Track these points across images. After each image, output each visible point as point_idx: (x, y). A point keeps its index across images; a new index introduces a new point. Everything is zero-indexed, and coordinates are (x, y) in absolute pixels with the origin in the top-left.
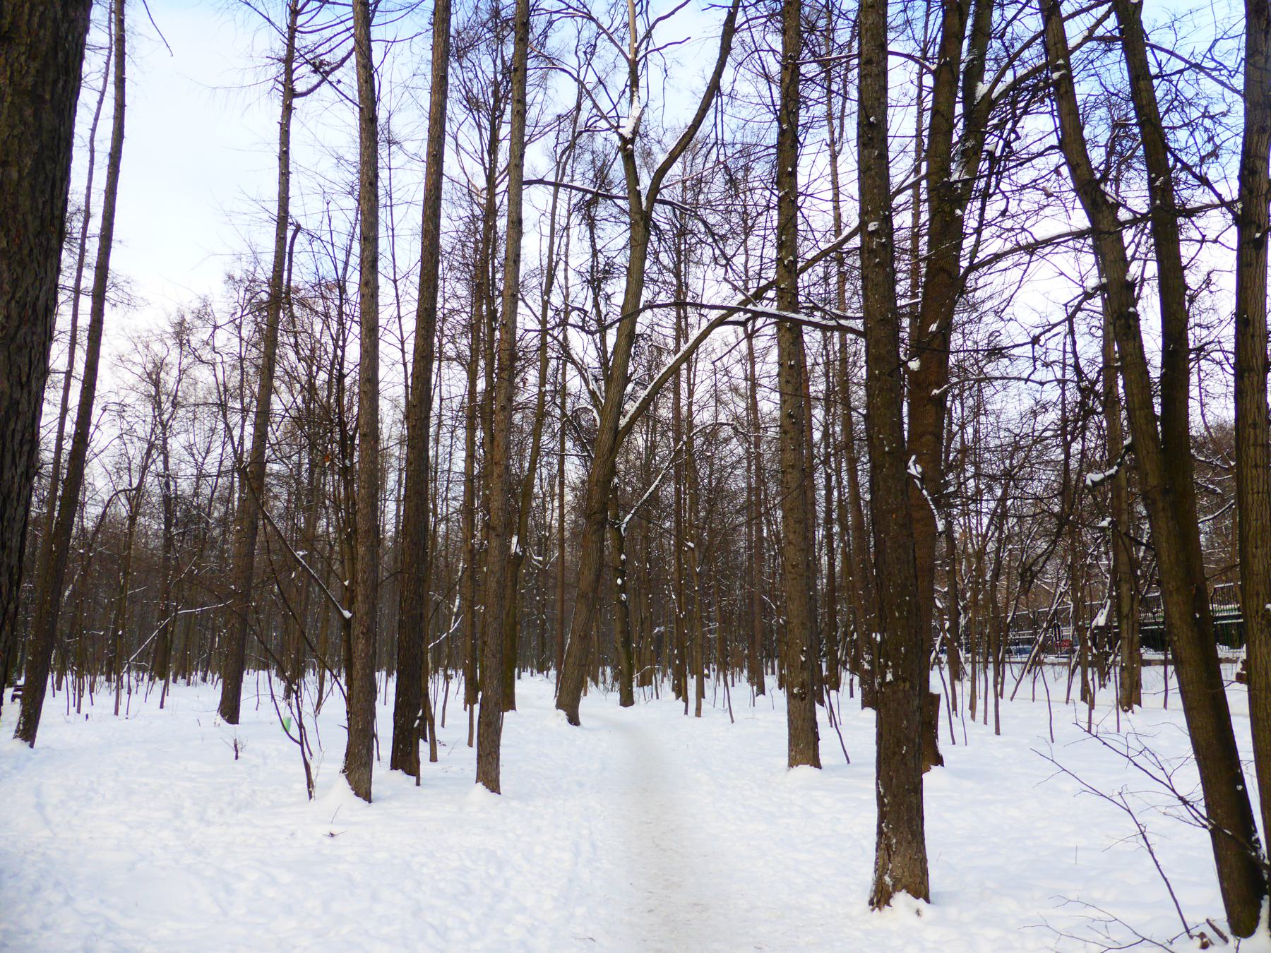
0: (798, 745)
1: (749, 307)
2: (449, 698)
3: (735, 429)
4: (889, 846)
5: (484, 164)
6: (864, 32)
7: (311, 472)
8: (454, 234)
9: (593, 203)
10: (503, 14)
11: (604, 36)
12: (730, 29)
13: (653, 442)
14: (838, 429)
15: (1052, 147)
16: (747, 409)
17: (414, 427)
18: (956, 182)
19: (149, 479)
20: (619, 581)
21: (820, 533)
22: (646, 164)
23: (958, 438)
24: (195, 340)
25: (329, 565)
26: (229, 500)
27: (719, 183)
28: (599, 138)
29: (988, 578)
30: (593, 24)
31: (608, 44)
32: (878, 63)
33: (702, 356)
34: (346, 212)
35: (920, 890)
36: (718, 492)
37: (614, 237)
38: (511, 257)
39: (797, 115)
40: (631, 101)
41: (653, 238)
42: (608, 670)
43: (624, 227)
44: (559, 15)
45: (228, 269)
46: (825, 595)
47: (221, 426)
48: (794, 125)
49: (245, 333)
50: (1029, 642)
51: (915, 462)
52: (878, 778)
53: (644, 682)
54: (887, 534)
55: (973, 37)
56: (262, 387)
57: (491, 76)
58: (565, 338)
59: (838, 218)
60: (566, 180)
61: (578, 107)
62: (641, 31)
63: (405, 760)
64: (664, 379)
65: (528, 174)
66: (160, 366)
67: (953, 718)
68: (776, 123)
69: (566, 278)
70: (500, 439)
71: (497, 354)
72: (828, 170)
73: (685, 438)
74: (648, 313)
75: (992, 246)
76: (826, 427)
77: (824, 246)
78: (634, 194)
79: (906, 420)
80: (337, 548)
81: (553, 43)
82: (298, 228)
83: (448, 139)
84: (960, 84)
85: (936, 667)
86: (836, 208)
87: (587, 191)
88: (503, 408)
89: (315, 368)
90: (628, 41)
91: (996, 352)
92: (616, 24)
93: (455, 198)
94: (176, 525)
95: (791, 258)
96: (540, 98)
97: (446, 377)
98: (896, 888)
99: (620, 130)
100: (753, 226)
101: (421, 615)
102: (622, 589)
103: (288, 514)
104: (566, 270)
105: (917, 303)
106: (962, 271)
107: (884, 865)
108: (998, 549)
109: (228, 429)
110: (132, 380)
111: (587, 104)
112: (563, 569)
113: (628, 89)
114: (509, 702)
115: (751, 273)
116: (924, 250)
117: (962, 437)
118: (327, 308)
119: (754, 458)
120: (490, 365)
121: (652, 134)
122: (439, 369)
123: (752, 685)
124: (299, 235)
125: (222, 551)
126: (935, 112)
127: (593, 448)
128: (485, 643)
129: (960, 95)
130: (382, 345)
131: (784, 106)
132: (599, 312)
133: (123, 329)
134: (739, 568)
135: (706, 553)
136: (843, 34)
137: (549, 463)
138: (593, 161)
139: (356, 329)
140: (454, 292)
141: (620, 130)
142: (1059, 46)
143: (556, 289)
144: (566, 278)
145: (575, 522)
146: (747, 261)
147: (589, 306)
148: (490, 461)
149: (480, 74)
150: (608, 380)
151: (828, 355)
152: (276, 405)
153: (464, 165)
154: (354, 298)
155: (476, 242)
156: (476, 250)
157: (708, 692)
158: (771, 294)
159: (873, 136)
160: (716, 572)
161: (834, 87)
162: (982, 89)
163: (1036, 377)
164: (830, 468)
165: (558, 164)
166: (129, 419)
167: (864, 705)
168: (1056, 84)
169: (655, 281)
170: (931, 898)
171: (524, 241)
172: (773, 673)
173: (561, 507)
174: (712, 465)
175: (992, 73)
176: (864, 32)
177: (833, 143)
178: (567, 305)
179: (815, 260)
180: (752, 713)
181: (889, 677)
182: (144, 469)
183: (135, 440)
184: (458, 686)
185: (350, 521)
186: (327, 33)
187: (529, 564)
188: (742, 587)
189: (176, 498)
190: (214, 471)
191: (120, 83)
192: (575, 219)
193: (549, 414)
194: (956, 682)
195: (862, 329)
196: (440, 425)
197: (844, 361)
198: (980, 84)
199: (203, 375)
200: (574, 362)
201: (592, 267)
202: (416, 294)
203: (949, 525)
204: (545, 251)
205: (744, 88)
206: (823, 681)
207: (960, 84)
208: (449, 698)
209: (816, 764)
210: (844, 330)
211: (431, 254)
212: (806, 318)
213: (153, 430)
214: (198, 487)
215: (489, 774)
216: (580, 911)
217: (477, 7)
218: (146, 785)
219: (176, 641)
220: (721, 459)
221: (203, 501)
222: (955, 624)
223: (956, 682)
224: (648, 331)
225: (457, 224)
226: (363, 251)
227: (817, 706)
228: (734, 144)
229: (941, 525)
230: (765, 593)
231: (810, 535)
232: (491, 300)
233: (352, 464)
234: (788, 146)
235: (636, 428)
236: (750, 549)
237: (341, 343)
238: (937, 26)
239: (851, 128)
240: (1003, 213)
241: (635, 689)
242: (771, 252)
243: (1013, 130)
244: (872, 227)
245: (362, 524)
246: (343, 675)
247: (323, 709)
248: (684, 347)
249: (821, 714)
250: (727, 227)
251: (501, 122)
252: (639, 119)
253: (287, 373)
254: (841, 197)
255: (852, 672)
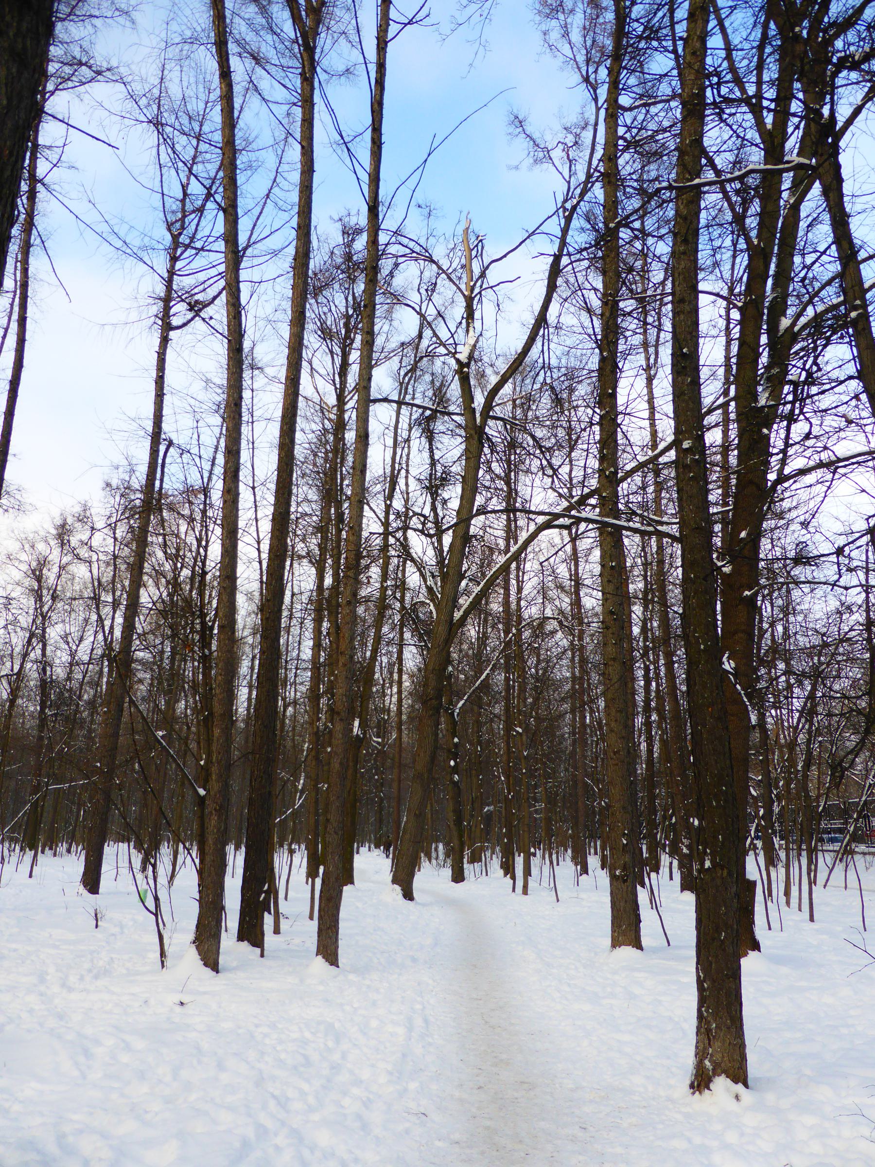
0: (620, 927)
1: (573, 513)
2: (292, 870)
3: (560, 623)
4: (708, 1031)
5: (335, 384)
6: (676, 275)
7: (172, 658)
8: (307, 446)
9: (432, 418)
10: (355, 258)
11: (443, 276)
12: (555, 271)
13: (484, 633)
14: (655, 624)
15: (850, 378)
16: (571, 604)
17: (267, 619)
18: (763, 407)
19: (29, 665)
20: (452, 763)
21: (639, 720)
22: (480, 384)
23: (768, 635)
24: (74, 541)
25: (186, 745)
26: (98, 684)
27: (546, 400)
28: (438, 362)
29: (799, 768)
30: (434, 266)
31: (447, 283)
32: (690, 302)
33: (530, 556)
34: (213, 427)
35: (739, 1076)
36: (544, 681)
37: (451, 448)
38: (359, 467)
39: (616, 344)
40: (467, 331)
41: (486, 450)
42: (441, 846)
43: (460, 440)
44: (404, 259)
45: (106, 478)
46: (644, 779)
47: (94, 617)
48: (613, 354)
49: (119, 534)
50: (840, 831)
51: (729, 658)
52: (697, 963)
53: (475, 859)
54: (704, 726)
55: (776, 277)
56: (132, 582)
57: (343, 310)
58: (406, 539)
59: (654, 434)
60: (408, 398)
61: (420, 336)
62: (477, 271)
63: (251, 933)
64: (495, 577)
65: (374, 394)
66: (43, 563)
67: (769, 903)
68: (597, 351)
69: (407, 485)
70: (345, 632)
71: (342, 549)
72: (645, 391)
73: (514, 631)
74: (482, 518)
75: (796, 464)
76: (644, 622)
77: (641, 459)
78: (469, 410)
79: (719, 617)
80: (193, 729)
81: (398, 282)
82: (170, 444)
83: (305, 364)
84: (765, 317)
85: (751, 853)
86: (653, 425)
87: (425, 408)
88: (349, 603)
89: (179, 565)
90: (465, 279)
91: (802, 559)
92: (454, 266)
93: (309, 414)
94: (51, 706)
95: (612, 469)
96: (386, 328)
97: (296, 573)
98: (716, 1073)
99: (457, 356)
100: (576, 441)
101: (270, 793)
102: (455, 770)
103: (150, 697)
104: (407, 477)
105: (728, 511)
106: (769, 484)
107: (705, 1049)
108: (809, 742)
109: (100, 620)
110: (17, 575)
111: (427, 333)
112: (400, 751)
113: (464, 321)
114: (348, 877)
115: (575, 481)
116: (733, 460)
117: (773, 635)
118: (192, 511)
119: (577, 649)
120: (337, 563)
121: (486, 359)
122: (291, 565)
123: (576, 865)
124: (171, 449)
125: (90, 731)
126: (743, 342)
127: (429, 637)
128: (328, 820)
129: (765, 327)
130: (240, 545)
131: (605, 336)
132: (436, 515)
133: (13, 531)
134: (564, 752)
135: (533, 737)
136: (657, 275)
137: (389, 653)
138: (432, 382)
139: (218, 531)
140: (306, 497)
141: (457, 356)
142: (856, 288)
143: (397, 495)
144: (407, 485)
145: (412, 706)
146: (571, 471)
147: (427, 511)
148: (335, 652)
149: (333, 308)
150: (444, 577)
151: (645, 557)
152: (144, 598)
153: (318, 386)
154: (217, 504)
155: (326, 453)
156: (326, 460)
157: (534, 871)
158: (593, 501)
159: (686, 365)
160: (543, 755)
161: (650, 319)
162: (785, 323)
163: (842, 582)
164: (649, 660)
165: (401, 384)
166: (14, 611)
167: (683, 889)
168: (854, 323)
169: (488, 488)
170: (750, 1083)
171: (371, 451)
172: (596, 853)
173: (400, 692)
174: (538, 656)
175: (794, 309)
176: (676, 275)
177: (648, 368)
178: (407, 509)
179: (633, 471)
180: (579, 893)
181: (708, 864)
182: (25, 655)
183: (18, 630)
184: (301, 859)
185: (207, 699)
186: (202, 276)
187: (369, 746)
188: (566, 770)
189: (52, 681)
190: (86, 658)
191: (22, 321)
192: (416, 433)
193: (389, 607)
194: (771, 868)
195: (677, 534)
196: (291, 617)
197: (661, 562)
198: (783, 318)
199: (81, 571)
200: (413, 560)
201: (431, 475)
202: (272, 499)
203: (762, 717)
204: (389, 460)
205: (569, 320)
206: (643, 863)
207: (765, 317)
208: (292, 870)
209: (640, 947)
210: (661, 535)
211: (287, 465)
212: (625, 524)
213: (34, 621)
214: (71, 672)
215: (328, 947)
216: (413, 1086)
217: (332, 253)
218: (15, 950)
219: (45, 814)
220: (547, 650)
221: (75, 684)
222: (769, 812)
223: (771, 868)
224: (481, 533)
225: (310, 436)
226: (226, 463)
227: (639, 887)
228: (559, 368)
229: (754, 719)
230: (587, 776)
231: (630, 722)
232: (339, 505)
233: (211, 653)
234: (608, 373)
235: (469, 620)
236: (574, 735)
237: (204, 543)
238: (743, 267)
239: (666, 354)
240: (807, 436)
241: (466, 866)
242: (594, 463)
243: (815, 363)
244: (686, 445)
245: (218, 708)
246: (195, 848)
247: (176, 881)
248: (513, 549)
249: (643, 896)
250: (553, 440)
251: (351, 349)
252: (475, 346)
253: (154, 569)
254: (657, 416)
255: (671, 855)
